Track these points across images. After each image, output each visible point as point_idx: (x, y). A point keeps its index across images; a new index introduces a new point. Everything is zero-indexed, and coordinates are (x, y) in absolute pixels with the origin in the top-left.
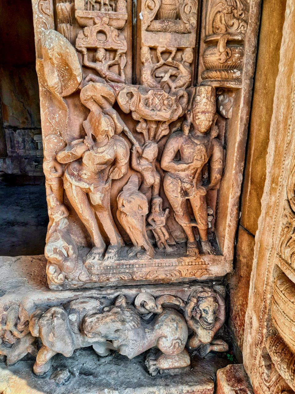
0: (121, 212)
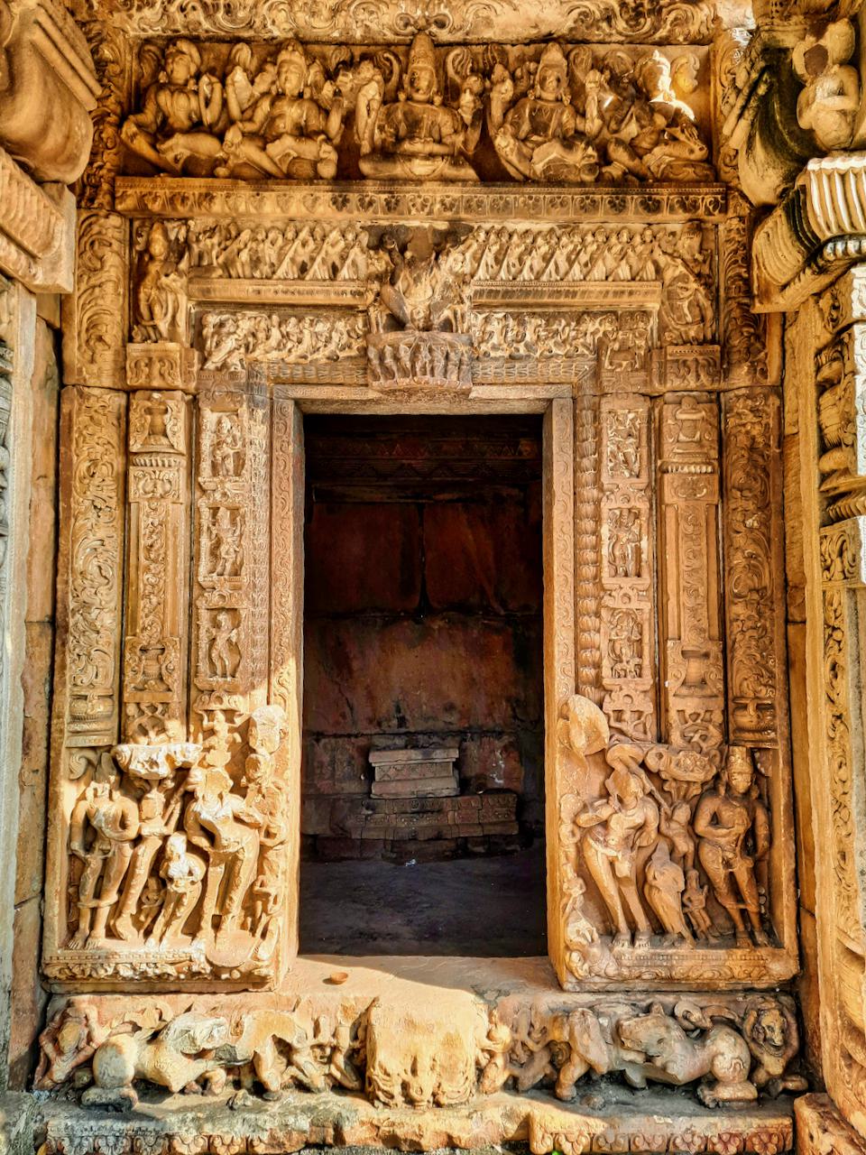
0: (651, 886)
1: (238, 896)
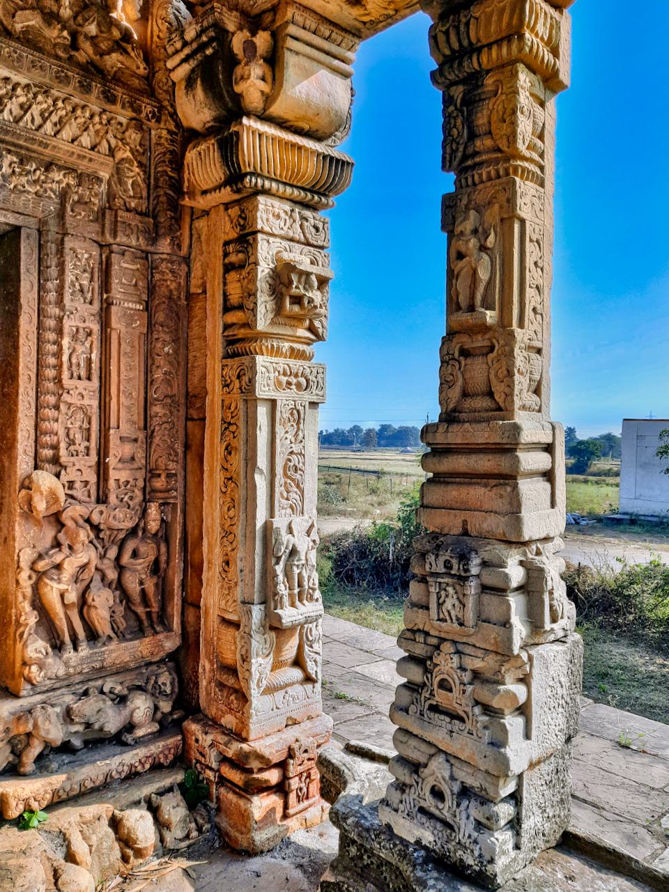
0: (89, 607)
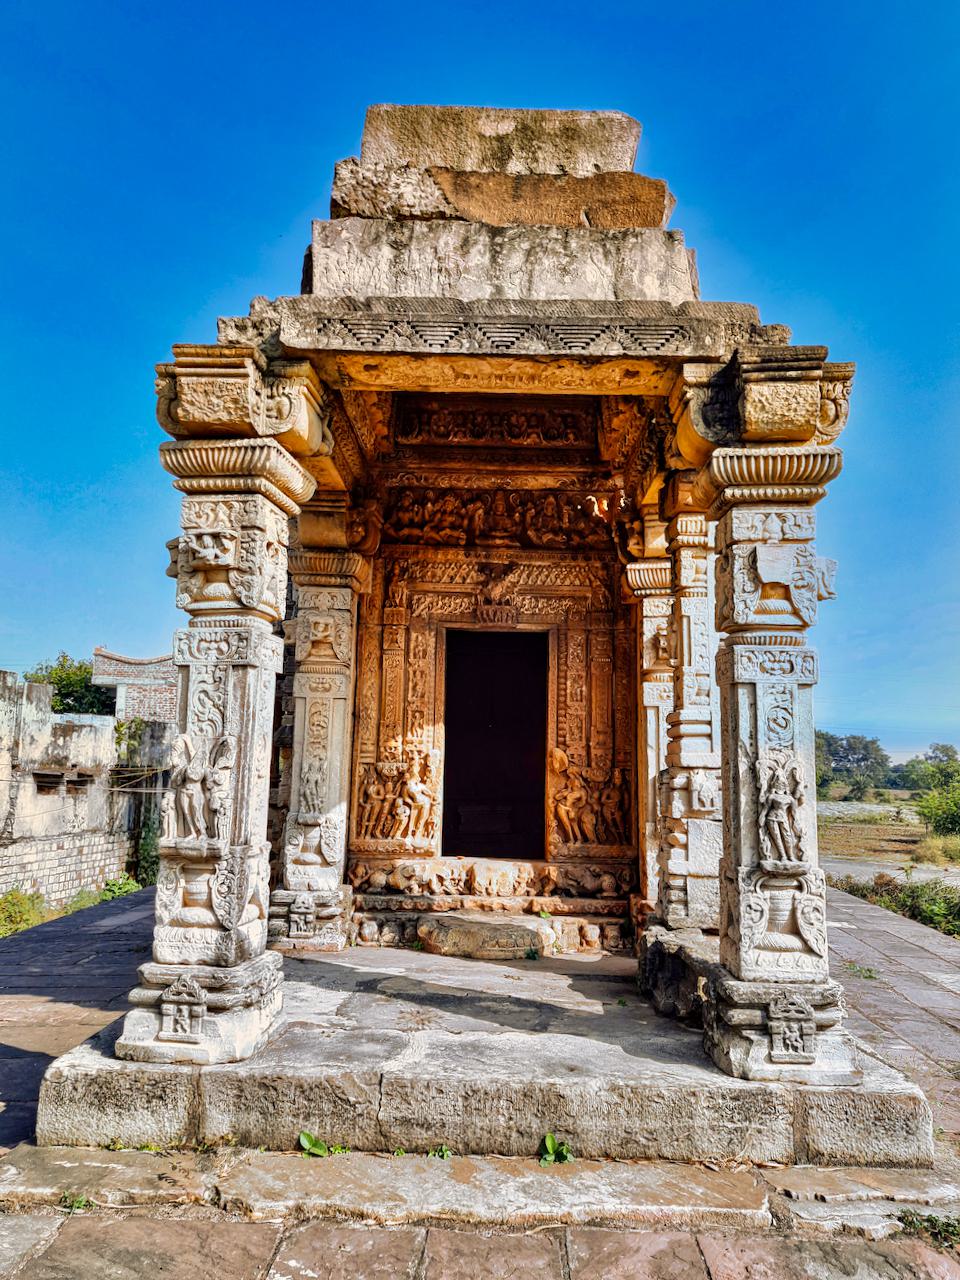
1: (422, 822)
